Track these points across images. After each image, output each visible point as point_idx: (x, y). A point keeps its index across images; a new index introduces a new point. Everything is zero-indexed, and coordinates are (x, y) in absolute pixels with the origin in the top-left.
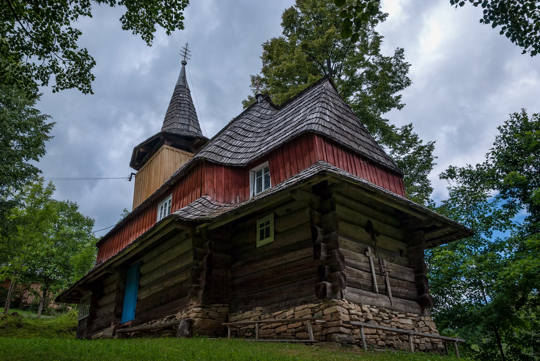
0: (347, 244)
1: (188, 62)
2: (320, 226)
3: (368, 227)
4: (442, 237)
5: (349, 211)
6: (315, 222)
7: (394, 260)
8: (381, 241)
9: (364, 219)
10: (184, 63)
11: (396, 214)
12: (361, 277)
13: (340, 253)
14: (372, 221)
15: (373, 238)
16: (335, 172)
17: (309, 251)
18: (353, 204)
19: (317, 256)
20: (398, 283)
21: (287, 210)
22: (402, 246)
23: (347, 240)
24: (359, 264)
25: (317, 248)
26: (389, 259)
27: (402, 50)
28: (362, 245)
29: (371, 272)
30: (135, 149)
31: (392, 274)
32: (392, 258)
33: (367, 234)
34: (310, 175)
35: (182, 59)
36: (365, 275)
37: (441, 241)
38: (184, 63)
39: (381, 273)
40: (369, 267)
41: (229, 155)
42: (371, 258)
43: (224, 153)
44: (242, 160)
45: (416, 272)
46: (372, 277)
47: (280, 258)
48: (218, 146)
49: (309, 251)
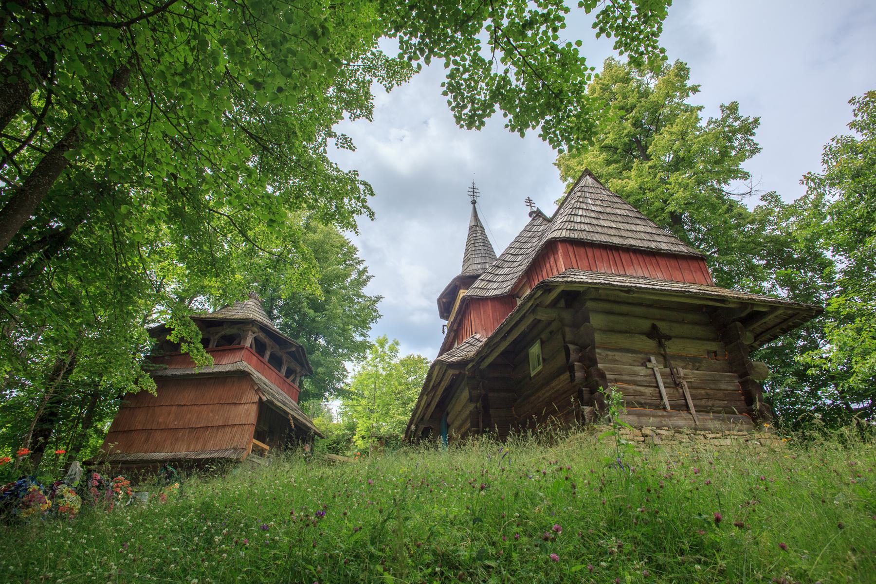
0: (616, 358)
1: (477, 199)
2: (573, 343)
3: (653, 333)
4: (781, 323)
5: (621, 319)
6: (567, 339)
7: (700, 367)
8: (672, 347)
9: (646, 325)
10: (474, 202)
11: (697, 309)
12: (641, 394)
13: (599, 370)
14: (656, 323)
15: (661, 345)
16: (566, 279)
17: (566, 376)
18: (625, 309)
19: (572, 377)
20: (707, 394)
21: (551, 333)
22: (713, 346)
23: (616, 353)
24: (638, 378)
25: (571, 369)
26: (690, 367)
27: (352, 148)
28: (642, 356)
29: (658, 387)
30: (439, 300)
31: (694, 385)
32: (697, 364)
33: (651, 341)
34: (643, 286)
35: (471, 199)
36: (648, 391)
37: (782, 329)
38: (474, 202)
39: (675, 384)
40: (654, 380)
41: (495, 286)
42: (656, 369)
43: (490, 285)
44: (507, 287)
45: (740, 377)
46: (660, 392)
47: (548, 388)
48: (483, 280)
49: (566, 376)
